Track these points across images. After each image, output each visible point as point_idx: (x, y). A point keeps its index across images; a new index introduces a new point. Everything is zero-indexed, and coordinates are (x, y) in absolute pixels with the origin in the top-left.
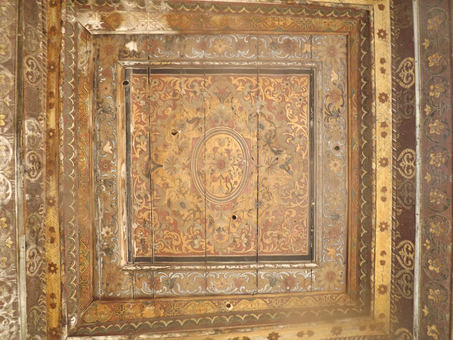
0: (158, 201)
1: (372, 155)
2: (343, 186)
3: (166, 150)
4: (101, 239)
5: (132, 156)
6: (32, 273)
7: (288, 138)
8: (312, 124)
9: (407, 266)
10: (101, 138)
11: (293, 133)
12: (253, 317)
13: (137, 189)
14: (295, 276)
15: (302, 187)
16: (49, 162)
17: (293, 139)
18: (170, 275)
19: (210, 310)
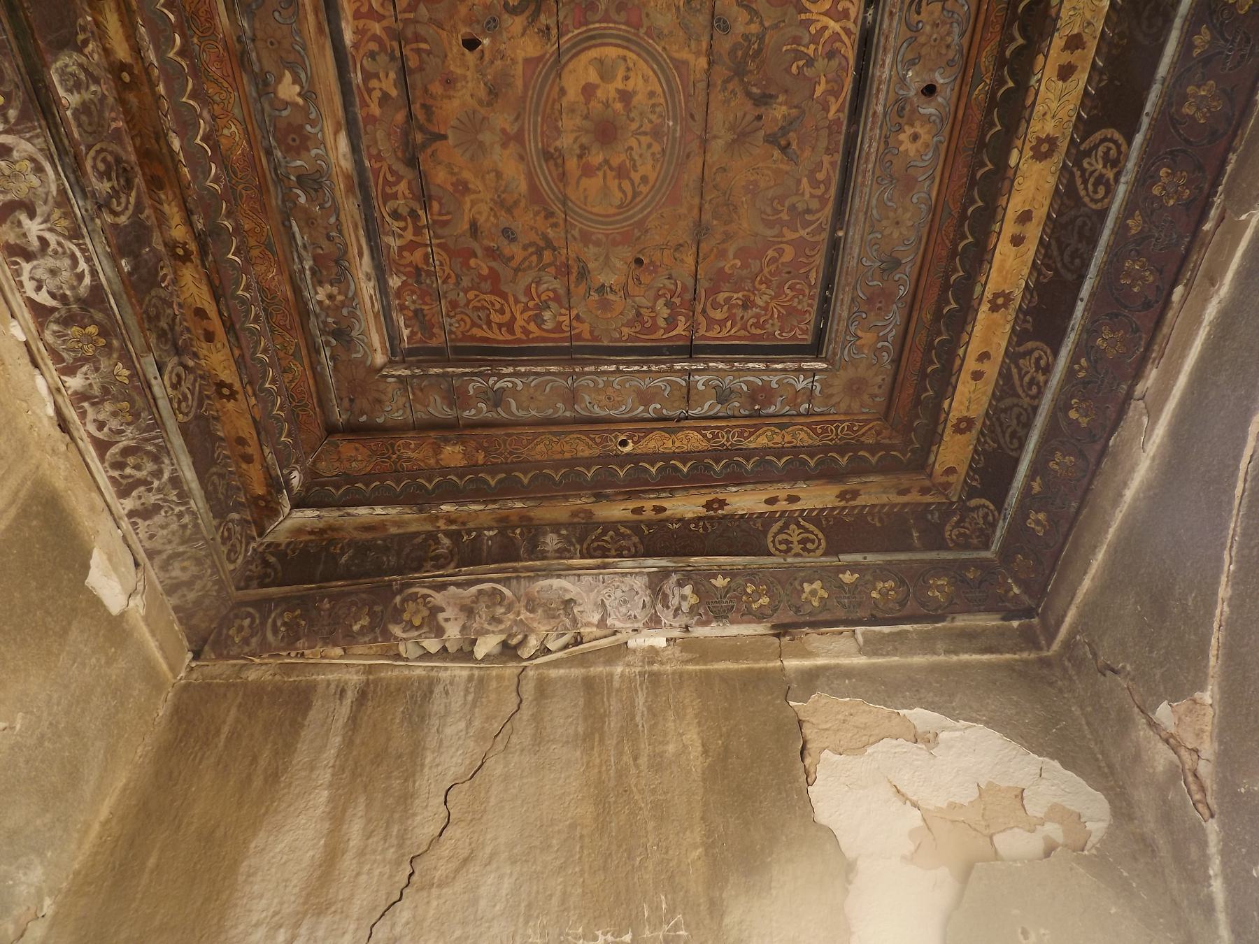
0: (445, 224)
1: (1017, 128)
2: (925, 191)
3: (451, 93)
4: (318, 310)
5: (360, 113)
6: (187, 414)
7: (796, 59)
8: (870, 18)
9: (1027, 395)
10: (265, 62)
11: (812, 47)
12: (675, 468)
13: (387, 198)
14: (774, 386)
15: (819, 192)
16: (145, 155)
17: (810, 62)
18: (491, 382)
19: (583, 451)
